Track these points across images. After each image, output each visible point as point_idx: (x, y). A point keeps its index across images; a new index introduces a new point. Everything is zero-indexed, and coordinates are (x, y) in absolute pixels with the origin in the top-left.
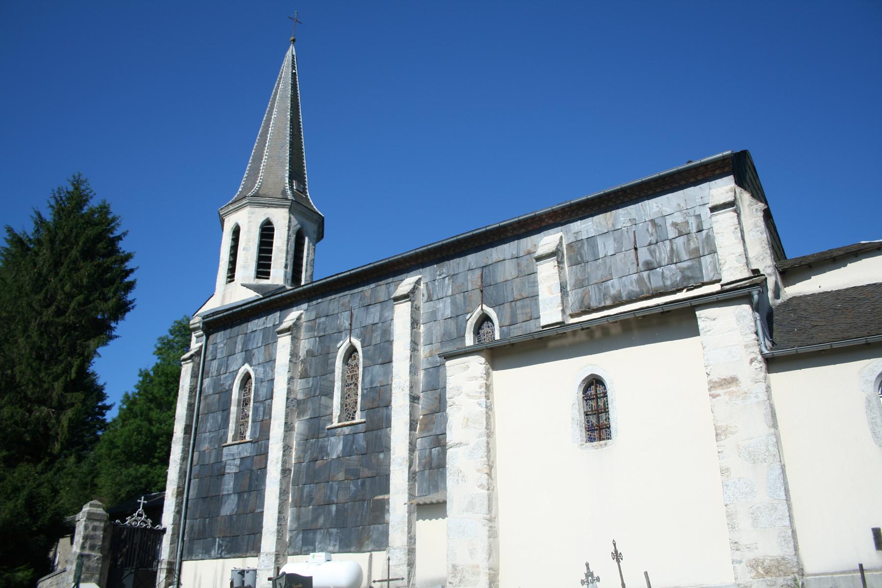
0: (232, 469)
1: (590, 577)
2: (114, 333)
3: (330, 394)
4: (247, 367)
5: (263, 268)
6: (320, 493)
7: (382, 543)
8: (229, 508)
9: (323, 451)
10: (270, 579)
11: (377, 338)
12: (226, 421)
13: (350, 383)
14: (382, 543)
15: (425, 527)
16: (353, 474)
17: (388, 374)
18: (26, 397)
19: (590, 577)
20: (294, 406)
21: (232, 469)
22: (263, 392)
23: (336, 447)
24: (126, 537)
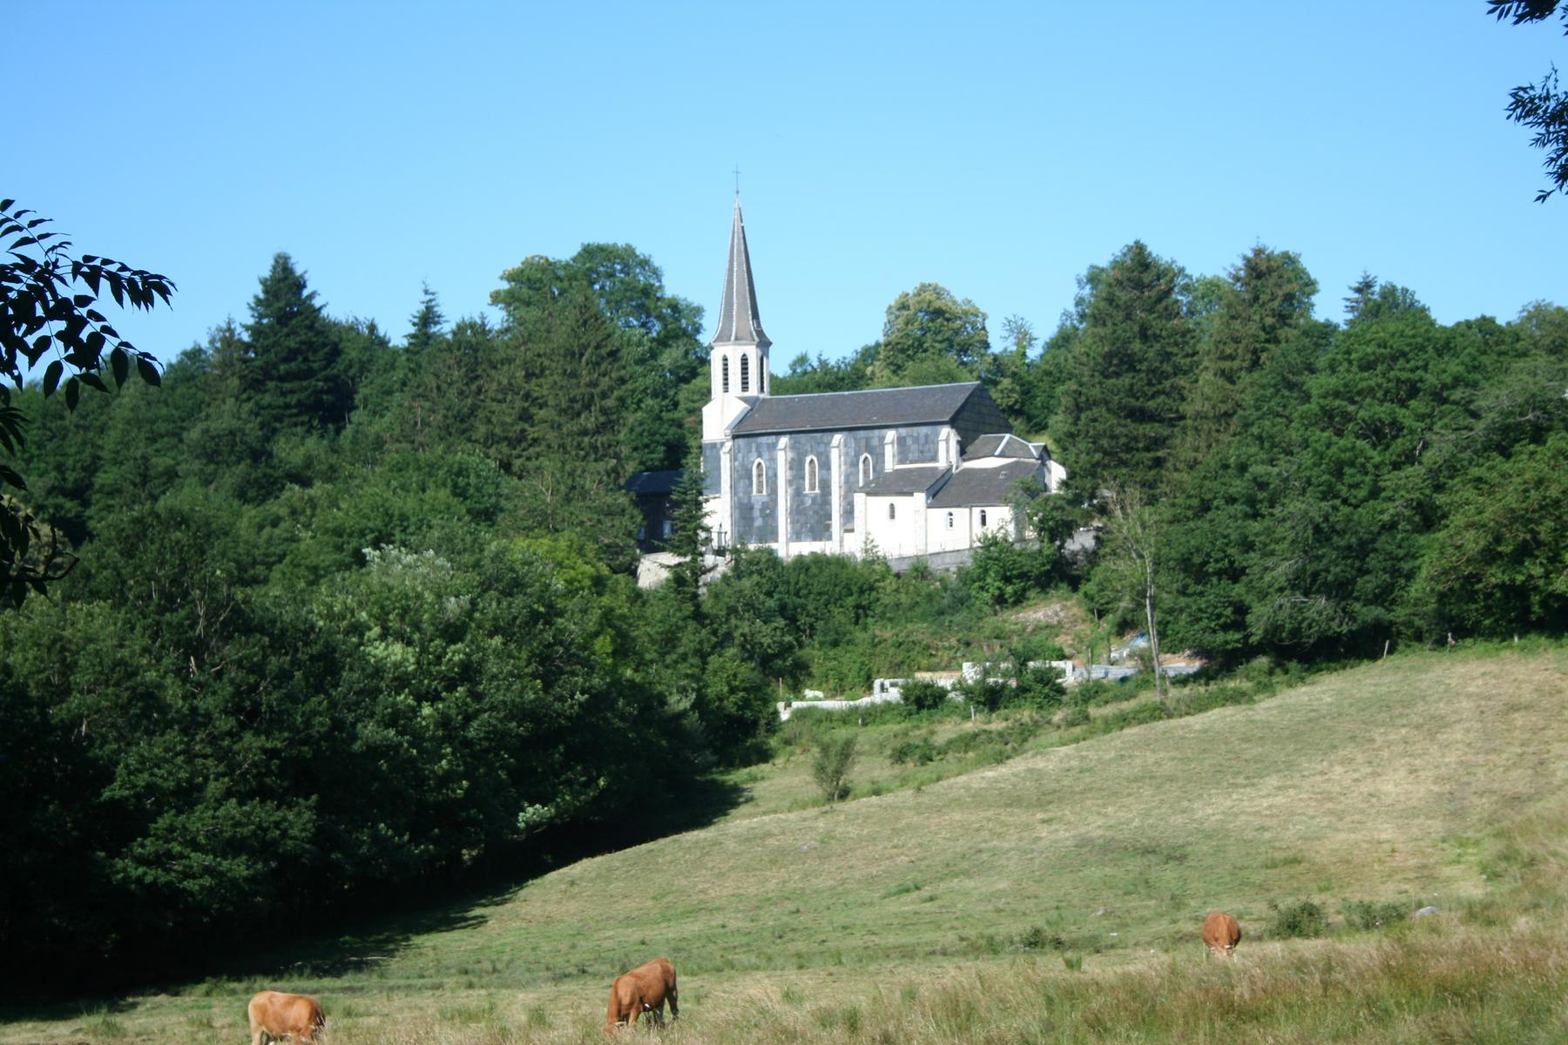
0: (757, 506)
1: (7, 204)
2: (479, 322)
3: (803, 479)
4: (759, 460)
5: (745, 385)
6: (802, 519)
7: (830, 538)
8: (758, 522)
9: (802, 503)
10: (389, 999)
11: (823, 459)
12: (751, 484)
13: (813, 473)
14: (830, 538)
15: (847, 535)
16: (816, 513)
17: (830, 474)
18: (220, 376)
19: (7, 204)
20: (790, 482)
21: (757, 506)
22: (770, 473)
23: (809, 502)
24: (189, 660)
